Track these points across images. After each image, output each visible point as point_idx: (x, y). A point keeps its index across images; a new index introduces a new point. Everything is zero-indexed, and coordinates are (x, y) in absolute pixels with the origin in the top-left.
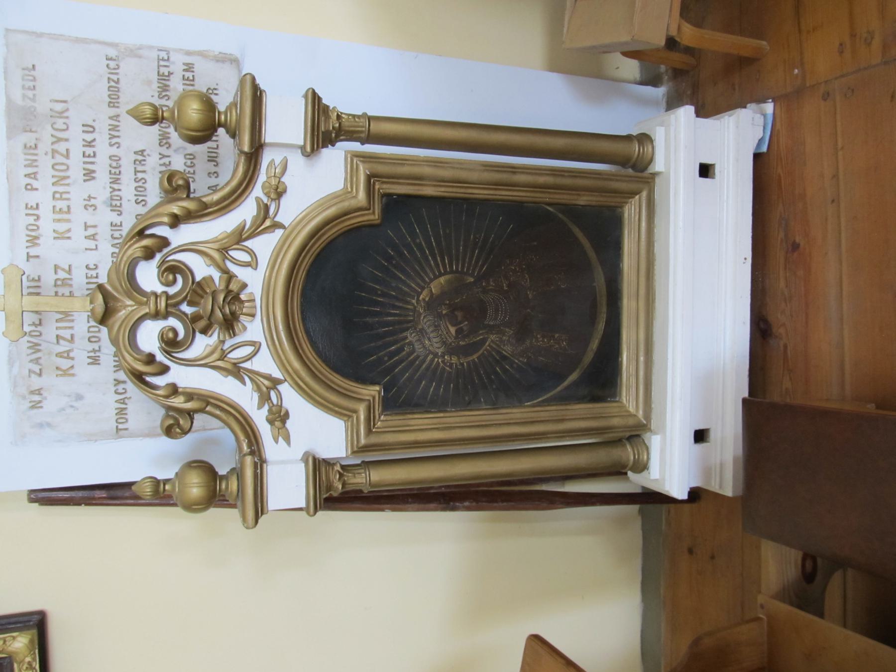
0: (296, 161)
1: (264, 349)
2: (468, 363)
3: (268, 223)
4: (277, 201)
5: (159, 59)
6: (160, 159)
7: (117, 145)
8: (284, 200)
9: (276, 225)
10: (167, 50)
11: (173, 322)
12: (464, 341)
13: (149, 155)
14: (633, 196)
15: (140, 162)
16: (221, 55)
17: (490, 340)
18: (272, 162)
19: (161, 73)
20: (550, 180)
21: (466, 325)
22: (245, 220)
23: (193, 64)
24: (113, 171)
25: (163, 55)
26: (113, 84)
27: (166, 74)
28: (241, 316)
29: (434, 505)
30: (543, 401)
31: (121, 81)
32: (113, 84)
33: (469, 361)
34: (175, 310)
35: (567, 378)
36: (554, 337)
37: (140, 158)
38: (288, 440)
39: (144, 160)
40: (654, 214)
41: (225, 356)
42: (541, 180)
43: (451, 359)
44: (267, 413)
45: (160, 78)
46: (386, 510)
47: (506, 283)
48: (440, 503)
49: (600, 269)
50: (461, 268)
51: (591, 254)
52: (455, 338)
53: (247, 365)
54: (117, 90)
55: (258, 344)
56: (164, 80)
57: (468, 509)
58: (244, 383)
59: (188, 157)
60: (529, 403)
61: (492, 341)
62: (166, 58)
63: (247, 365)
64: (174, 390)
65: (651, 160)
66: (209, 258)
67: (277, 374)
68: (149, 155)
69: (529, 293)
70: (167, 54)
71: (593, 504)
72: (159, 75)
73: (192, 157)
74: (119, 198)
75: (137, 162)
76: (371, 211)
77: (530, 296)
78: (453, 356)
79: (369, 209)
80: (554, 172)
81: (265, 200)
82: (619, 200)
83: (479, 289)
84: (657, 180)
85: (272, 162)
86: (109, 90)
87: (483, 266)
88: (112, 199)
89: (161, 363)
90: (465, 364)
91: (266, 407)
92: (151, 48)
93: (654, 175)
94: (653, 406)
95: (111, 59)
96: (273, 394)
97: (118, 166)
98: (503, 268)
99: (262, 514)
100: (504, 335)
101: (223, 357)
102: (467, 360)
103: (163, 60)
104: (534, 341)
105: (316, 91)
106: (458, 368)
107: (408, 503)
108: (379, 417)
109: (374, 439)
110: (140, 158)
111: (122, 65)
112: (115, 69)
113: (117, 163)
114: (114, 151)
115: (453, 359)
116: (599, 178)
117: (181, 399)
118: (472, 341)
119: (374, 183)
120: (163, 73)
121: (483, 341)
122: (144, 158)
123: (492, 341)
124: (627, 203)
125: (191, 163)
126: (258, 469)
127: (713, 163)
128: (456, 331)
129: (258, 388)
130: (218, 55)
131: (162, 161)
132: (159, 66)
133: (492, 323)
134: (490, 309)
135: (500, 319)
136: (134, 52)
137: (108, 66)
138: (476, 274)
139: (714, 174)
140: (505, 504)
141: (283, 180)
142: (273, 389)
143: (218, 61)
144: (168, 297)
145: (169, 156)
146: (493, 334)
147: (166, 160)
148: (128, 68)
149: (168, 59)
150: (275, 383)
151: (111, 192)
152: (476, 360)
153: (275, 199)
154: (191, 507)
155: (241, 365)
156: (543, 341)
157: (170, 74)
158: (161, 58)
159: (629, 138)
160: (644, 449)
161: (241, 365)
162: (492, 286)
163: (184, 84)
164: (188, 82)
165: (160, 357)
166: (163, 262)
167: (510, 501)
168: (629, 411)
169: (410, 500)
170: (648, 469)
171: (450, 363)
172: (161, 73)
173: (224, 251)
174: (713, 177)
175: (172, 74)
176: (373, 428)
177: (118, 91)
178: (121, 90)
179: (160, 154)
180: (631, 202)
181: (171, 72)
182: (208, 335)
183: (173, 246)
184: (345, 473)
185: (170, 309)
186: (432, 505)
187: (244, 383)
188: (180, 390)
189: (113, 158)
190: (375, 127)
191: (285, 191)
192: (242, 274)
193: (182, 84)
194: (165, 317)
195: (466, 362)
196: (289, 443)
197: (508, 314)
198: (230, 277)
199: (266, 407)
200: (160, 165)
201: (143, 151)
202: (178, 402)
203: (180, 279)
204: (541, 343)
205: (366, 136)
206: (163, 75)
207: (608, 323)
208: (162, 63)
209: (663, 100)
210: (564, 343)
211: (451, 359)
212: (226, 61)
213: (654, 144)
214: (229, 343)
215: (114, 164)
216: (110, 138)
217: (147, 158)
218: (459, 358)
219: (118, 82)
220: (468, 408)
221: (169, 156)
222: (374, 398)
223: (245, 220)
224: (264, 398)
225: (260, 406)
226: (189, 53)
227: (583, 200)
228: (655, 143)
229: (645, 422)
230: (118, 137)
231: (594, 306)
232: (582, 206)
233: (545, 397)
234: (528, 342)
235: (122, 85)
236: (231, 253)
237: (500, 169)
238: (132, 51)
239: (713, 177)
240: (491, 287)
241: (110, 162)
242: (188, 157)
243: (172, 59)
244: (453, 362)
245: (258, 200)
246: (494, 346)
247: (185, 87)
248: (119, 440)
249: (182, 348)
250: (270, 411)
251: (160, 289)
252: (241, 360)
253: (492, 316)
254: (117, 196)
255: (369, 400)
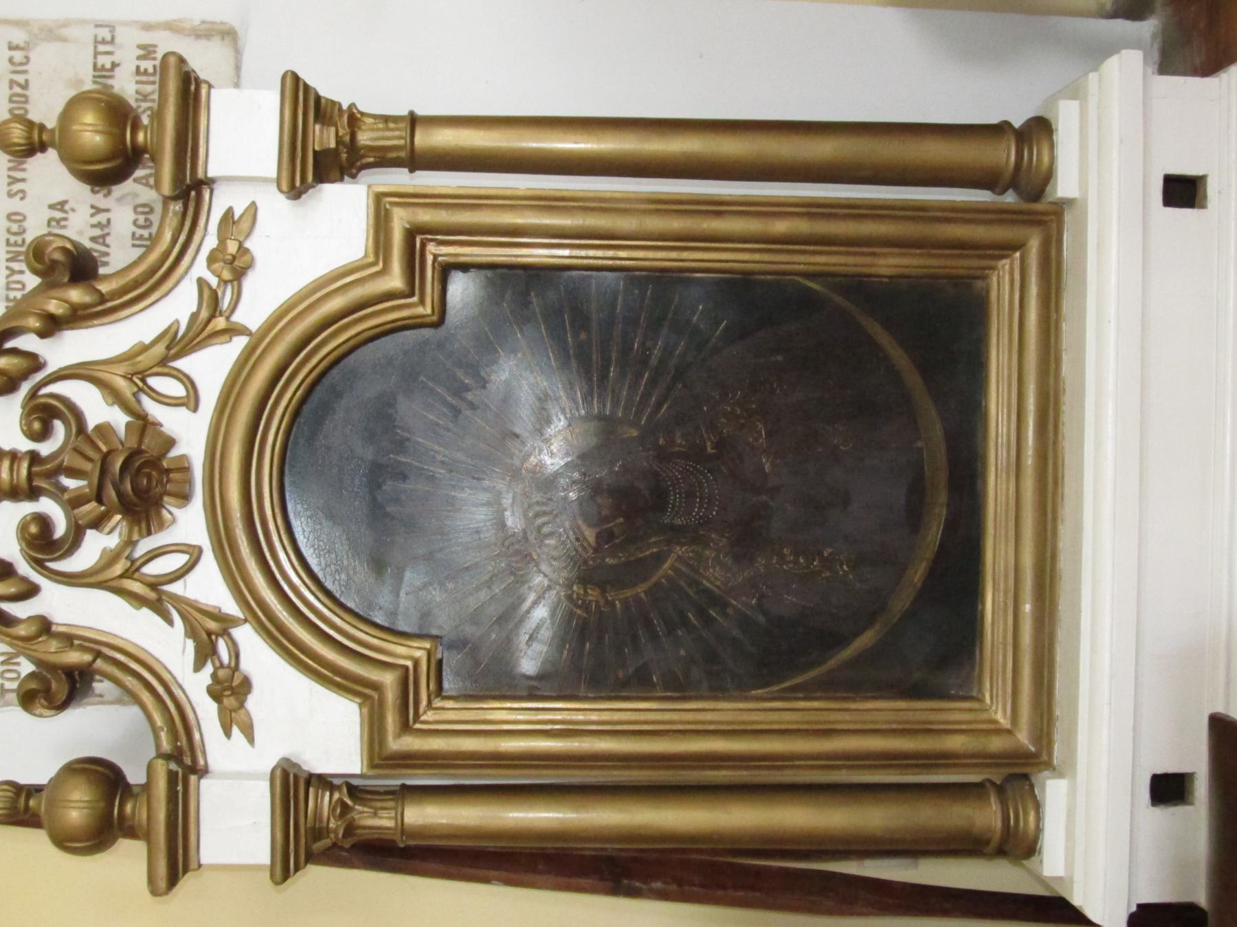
0: (274, 204)
1: (209, 562)
2: (625, 602)
3: (220, 323)
4: (235, 283)
5: (96, 42)
6: (92, 215)
7: (20, 195)
8: (249, 283)
9: (233, 331)
10: (113, 24)
11: (47, 506)
12: (614, 556)
13: (73, 210)
14: (1006, 252)
15: (58, 221)
16: (203, 27)
17: (676, 556)
18: (229, 213)
19: (99, 65)
20: (802, 226)
21: (621, 524)
22: (177, 321)
23: (155, 46)
24: (13, 239)
25: (104, 33)
26: (17, 90)
27: (108, 66)
28: (166, 499)
29: (590, 881)
30: (793, 689)
31: (31, 85)
32: (17, 90)
33: (626, 598)
34: (49, 484)
35: (849, 644)
36: (820, 554)
37: (58, 215)
38: (249, 732)
39: (65, 219)
40: (1059, 290)
41: (138, 569)
42: (780, 227)
43: (586, 592)
44: (209, 681)
45: (97, 74)
46: (493, 882)
47: (711, 441)
48: (602, 879)
49: (933, 413)
50: (610, 411)
51: (914, 380)
52: (596, 550)
53: (176, 588)
54: (23, 99)
55: (196, 551)
56: (104, 77)
57: (664, 896)
58: (170, 622)
59: (140, 209)
60: (760, 691)
61: (679, 558)
62: (108, 38)
63: (176, 588)
64: (44, 626)
65: (1049, 176)
66: (109, 391)
67: (231, 607)
68: (73, 210)
69: (764, 460)
70: (111, 31)
71: (945, 913)
72: (95, 68)
73: (147, 210)
74: (19, 286)
75: (54, 223)
76: (415, 299)
77: (767, 468)
78: (588, 586)
79: (412, 294)
80: (813, 209)
81: (214, 281)
82: (975, 263)
83: (651, 452)
84: (1068, 218)
85: (229, 213)
86: (11, 101)
87: (659, 406)
88: (8, 289)
89: (25, 580)
90: (617, 602)
91: (209, 669)
92: (82, 22)
93: (1060, 208)
94: (1058, 712)
95: (17, 48)
96: (222, 647)
97: (22, 231)
98: (705, 408)
99: (186, 870)
100: (707, 546)
101: (132, 572)
102: (621, 597)
103: (104, 42)
104: (774, 561)
105: (301, 75)
106: (601, 612)
107: (534, 871)
108: (429, 702)
109: (411, 743)
110: (58, 215)
111: (32, 55)
112: (21, 64)
113: (19, 226)
114: (15, 205)
115: (589, 591)
116: (922, 219)
117: (54, 645)
118: (632, 558)
119: (423, 245)
120: (103, 66)
121: (659, 559)
122: (63, 215)
123: (679, 558)
124: (993, 268)
125: (146, 220)
126: (177, 785)
127: (1201, 173)
128: (598, 536)
129: (191, 632)
130: (200, 25)
131: (95, 220)
132: (96, 54)
133: (680, 523)
134: (676, 494)
135: (698, 513)
136: (52, 33)
137: (11, 60)
138: (643, 422)
139: (1205, 197)
140: (741, 893)
141: (248, 245)
142: (222, 635)
143: (198, 37)
144: (34, 457)
145: (107, 210)
146: (683, 545)
147: (102, 218)
148: (44, 58)
149: (112, 41)
150: (226, 623)
151: (7, 277)
152: (643, 595)
153: (231, 281)
154: (65, 841)
155: (168, 588)
156: (796, 562)
157: (114, 65)
158: (100, 39)
159: (999, 130)
160: (1030, 805)
161: (168, 588)
162: (680, 445)
163: (137, 82)
164: (144, 78)
165: (24, 568)
166: (33, 394)
167: (752, 888)
168: (995, 722)
169: (540, 867)
170: (1040, 853)
171: (584, 601)
172: (99, 65)
173: (139, 377)
174: (1203, 206)
175: (118, 65)
176: (415, 722)
177: (26, 102)
178: (31, 99)
179: (92, 207)
180: (1003, 266)
181: (117, 62)
182: (107, 529)
183: (51, 368)
184: (357, 807)
185: (38, 482)
186: (583, 882)
187: (170, 622)
188: (54, 628)
189: (14, 217)
190: (428, 139)
191: (250, 266)
192: (171, 420)
193: (134, 82)
194: (33, 494)
195: (619, 600)
196: (251, 739)
197: (716, 508)
198: (143, 423)
199: (209, 669)
200: (93, 226)
201: (64, 203)
202: (51, 649)
203: (59, 427)
204: (791, 566)
205: (408, 155)
206: (103, 68)
207: (951, 526)
208: (102, 48)
209: (1152, 46)
210: (845, 567)
211: (586, 593)
212: (212, 36)
213: (1054, 137)
214: (144, 546)
215: (15, 228)
216: (9, 184)
217: (71, 215)
218: (603, 591)
219: (25, 86)
220: (623, 694)
221: (107, 210)
222: (416, 663)
223: (177, 321)
224: (205, 652)
225: (198, 666)
226: (148, 27)
227: (887, 264)
228: (1057, 135)
229: (1033, 749)
230: (23, 180)
231: (917, 491)
232: (890, 277)
233: (799, 680)
234: (761, 562)
235: (32, 92)
236: (152, 381)
237: (814, 210)
238: (50, 30)
239: (1203, 206)
240: (677, 449)
241: (8, 224)
242: (140, 209)
243: (117, 40)
244: (590, 598)
245: (201, 282)
246: (684, 569)
247: (141, 87)
248: (5, 708)
249: (55, 553)
250: (214, 676)
251: (25, 445)
252: (164, 579)
253: (680, 507)
254: (18, 282)
255: (406, 668)
